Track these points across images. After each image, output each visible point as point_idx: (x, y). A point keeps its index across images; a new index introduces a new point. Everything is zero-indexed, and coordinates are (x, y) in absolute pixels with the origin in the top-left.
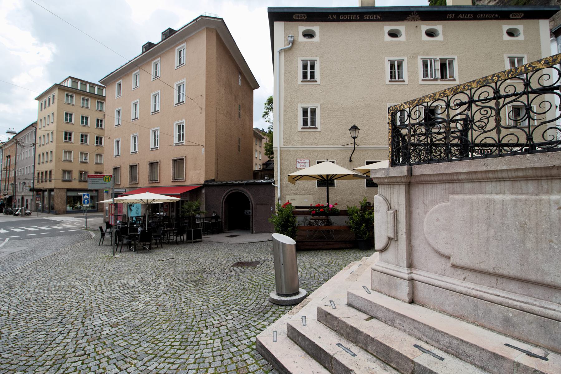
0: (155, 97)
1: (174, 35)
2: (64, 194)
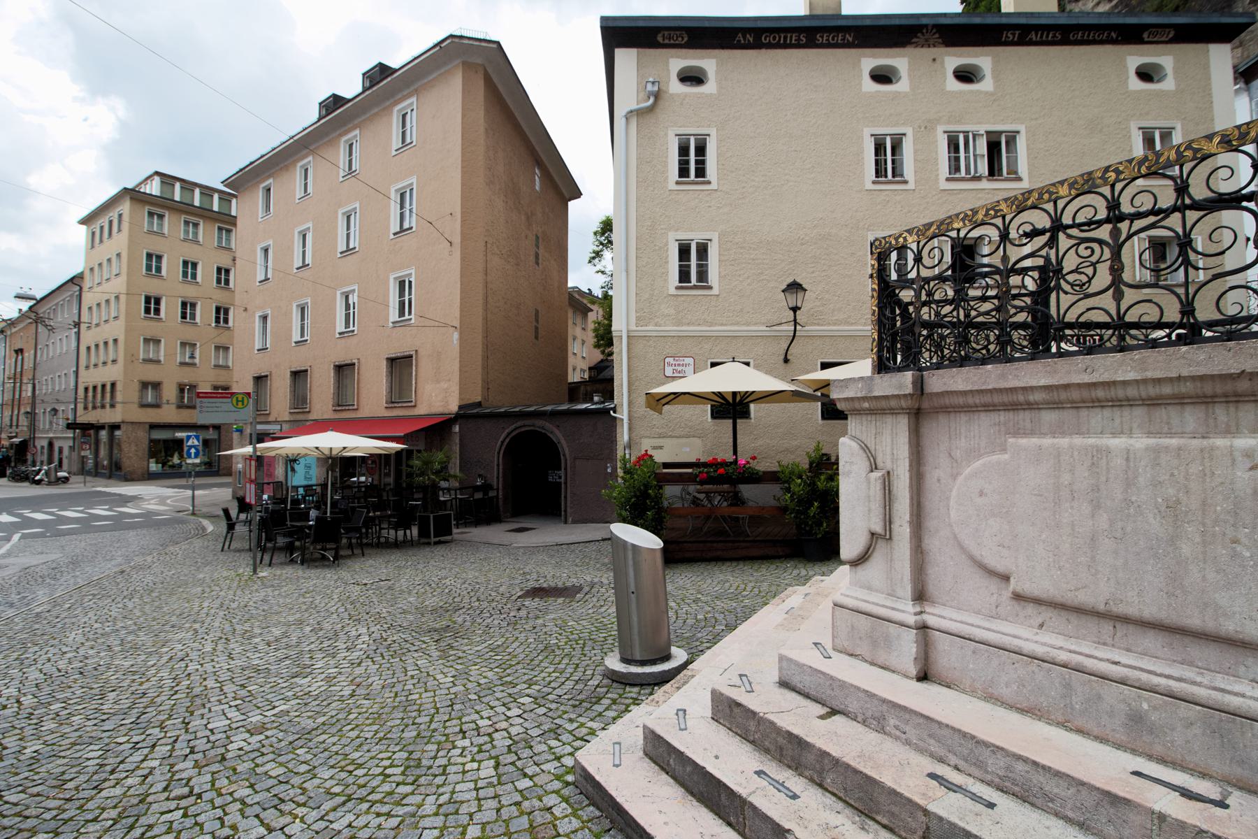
0: (348, 217)
1: (389, 79)
2: (143, 436)
